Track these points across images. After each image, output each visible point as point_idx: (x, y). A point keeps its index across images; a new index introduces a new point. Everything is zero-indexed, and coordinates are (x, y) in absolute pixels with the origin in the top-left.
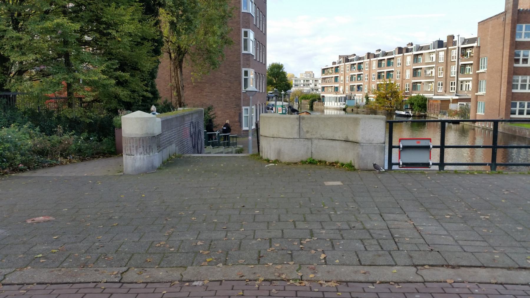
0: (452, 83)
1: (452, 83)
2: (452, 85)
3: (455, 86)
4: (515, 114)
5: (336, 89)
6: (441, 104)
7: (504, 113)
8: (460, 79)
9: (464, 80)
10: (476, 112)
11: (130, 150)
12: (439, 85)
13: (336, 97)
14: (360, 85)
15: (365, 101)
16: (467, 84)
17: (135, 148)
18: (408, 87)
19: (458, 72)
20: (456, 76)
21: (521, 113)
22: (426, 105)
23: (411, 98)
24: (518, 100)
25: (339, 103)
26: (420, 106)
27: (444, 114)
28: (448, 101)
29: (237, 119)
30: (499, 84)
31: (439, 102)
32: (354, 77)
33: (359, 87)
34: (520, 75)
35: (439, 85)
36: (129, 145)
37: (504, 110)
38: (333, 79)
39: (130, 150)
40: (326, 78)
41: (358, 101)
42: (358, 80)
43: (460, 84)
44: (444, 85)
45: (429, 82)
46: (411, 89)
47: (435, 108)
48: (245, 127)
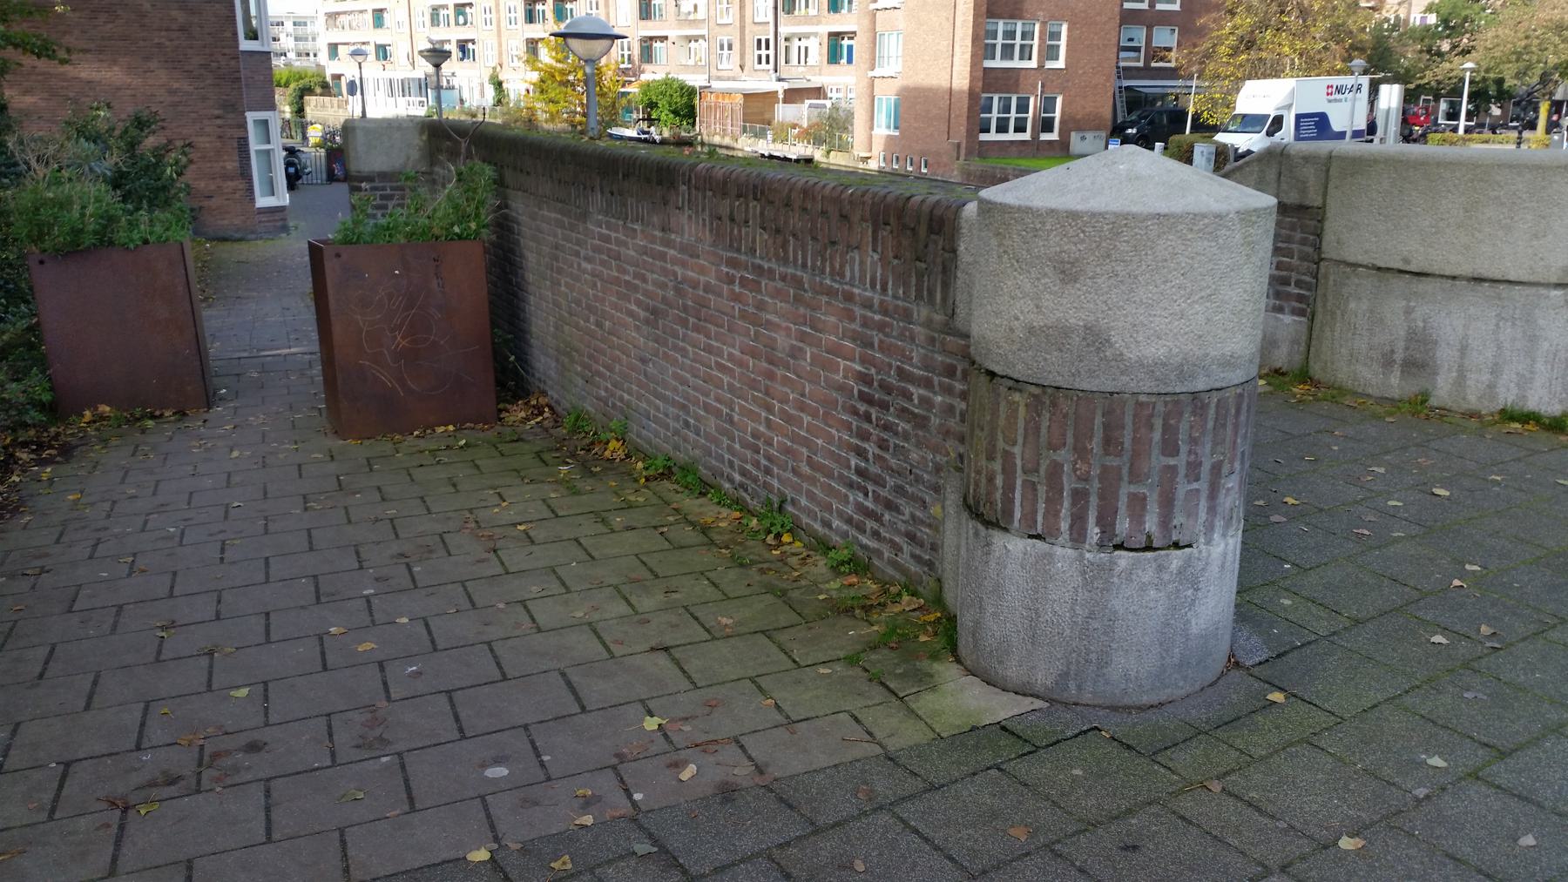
0: (759, 41)
1: (759, 41)
2: (759, 48)
3: (771, 52)
4: (988, 131)
5: (383, 52)
6: (745, 106)
7: (963, 129)
8: (784, 30)
9: (794, 35)
10: (872, 128)
11: (1167, 503)
12: (722, 48)
13: (1021, 58)
14: (467, 41)
15: (490, 92)
16: (803, 43)
17: (1203, 485)
18: (626, 53)
19: (776, 8)
20: (771, 18)
21: (1002, 128)
22: (693, 107)
23: (647, 87)
24: (996, 92)
25: (402, 101)
26: (675, 113)
27: (760, 135)
28: (770, 97)
29: (232, 165)
30: (946, 43)
31: (739, 99)
32: (442, 12)
33: (463, 46)
34: (1001, 17)
35: (722, 48)
36: (1157, 460)
37: (964, 120)
38: (369, 17)
39: (1167, 503)
40: (338, 14)
41: (465, 96)
42: (457, 24)
43: (782, 44)
44: (736, 46)
45: (689, 39)
46: (636, 59)
47: (723, 118)
48: (263, 195)
